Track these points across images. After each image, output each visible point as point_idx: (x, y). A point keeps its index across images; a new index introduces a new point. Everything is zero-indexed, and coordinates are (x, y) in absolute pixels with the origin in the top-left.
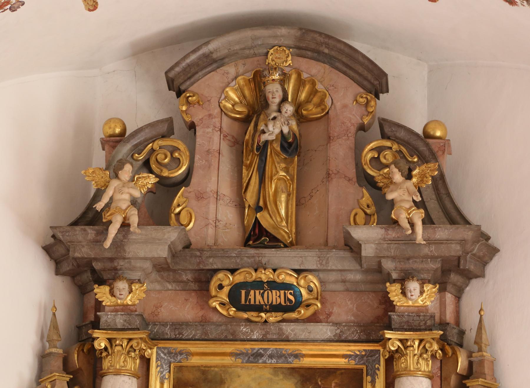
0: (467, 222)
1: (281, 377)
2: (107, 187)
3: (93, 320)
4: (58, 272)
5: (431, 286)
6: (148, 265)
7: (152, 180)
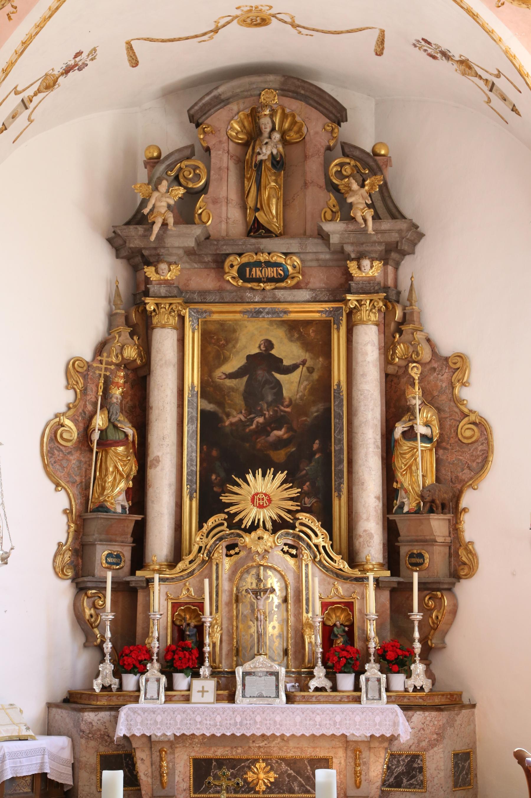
0: (404, 217)
1: (275, 326)
2: (150, 197)
3: (144, 290)
4: (118, 257)
5: (378, 262)
6: (181, 252)
7: (181, 191)
